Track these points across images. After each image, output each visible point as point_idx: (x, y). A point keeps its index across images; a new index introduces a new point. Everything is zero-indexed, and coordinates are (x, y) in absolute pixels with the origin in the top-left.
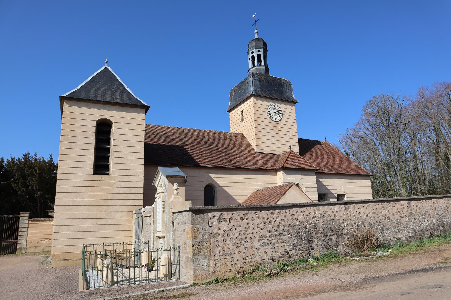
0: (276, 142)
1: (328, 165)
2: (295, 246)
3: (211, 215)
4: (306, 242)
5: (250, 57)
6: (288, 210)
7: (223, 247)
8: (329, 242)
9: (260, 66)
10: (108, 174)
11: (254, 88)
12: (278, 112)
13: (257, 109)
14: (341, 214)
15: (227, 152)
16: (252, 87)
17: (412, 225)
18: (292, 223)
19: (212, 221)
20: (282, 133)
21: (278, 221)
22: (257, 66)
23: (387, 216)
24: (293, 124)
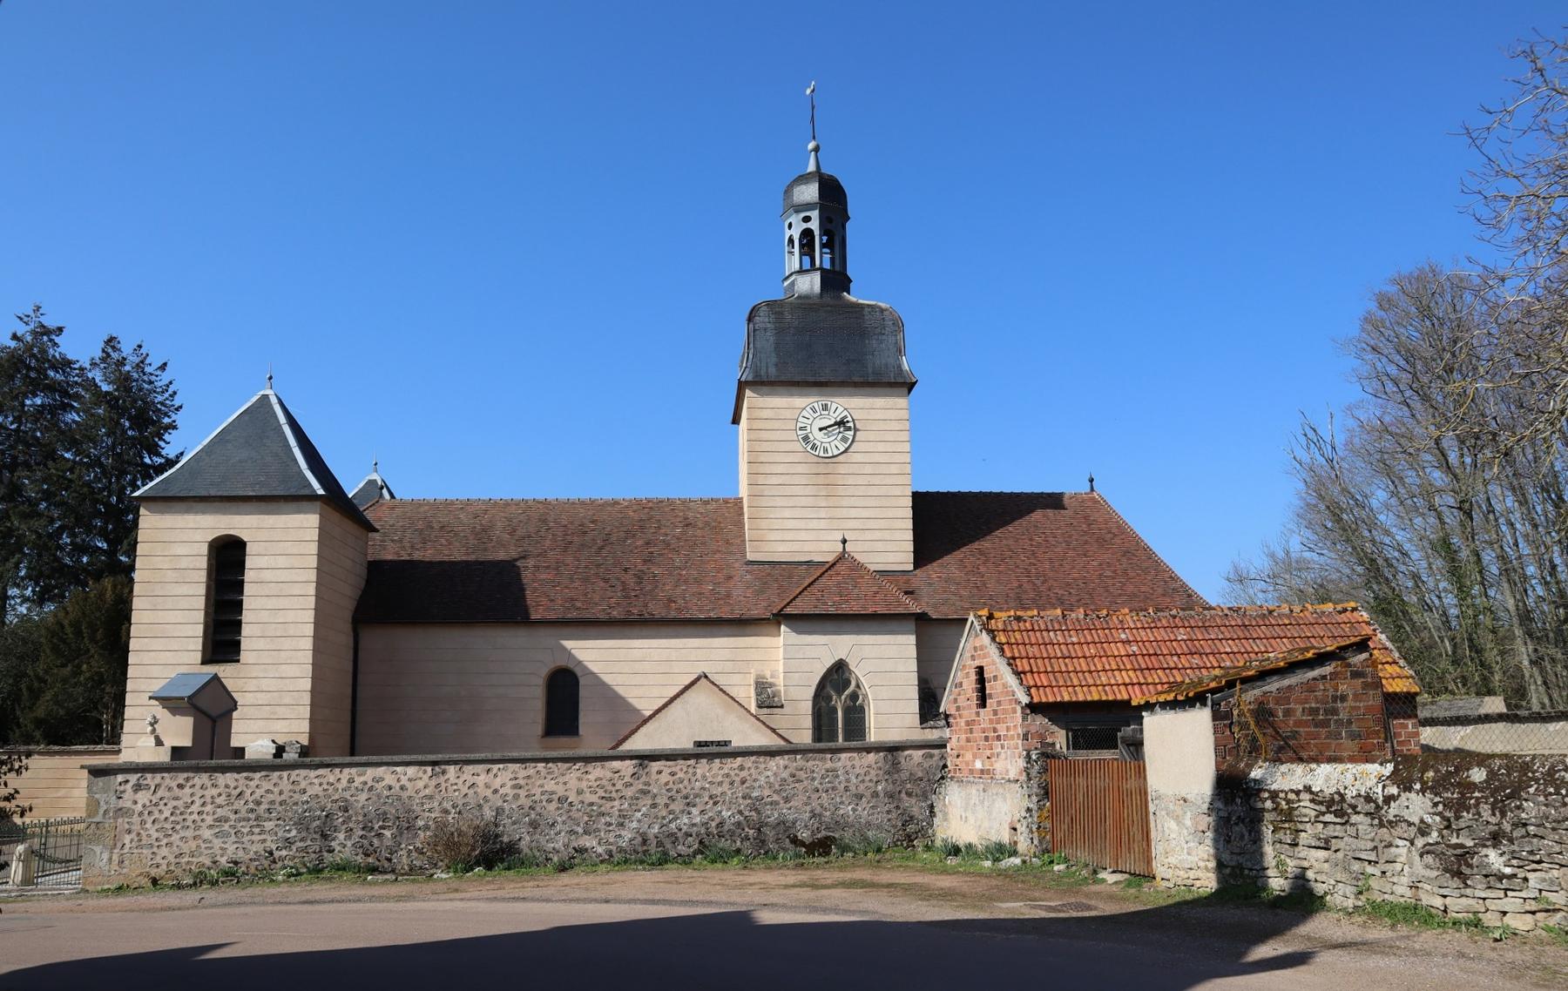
2: (289, 843)
3: (120, 778)
4: (317, 836)
6: (285, 774)
7: (139, 834)
8: (376, 842)
10: (238, 661)
14: (420, 784)
17: (639, 821)
18: (291, 797)
19: (122, 788)
21: (259, 792)
23: (560, 794)
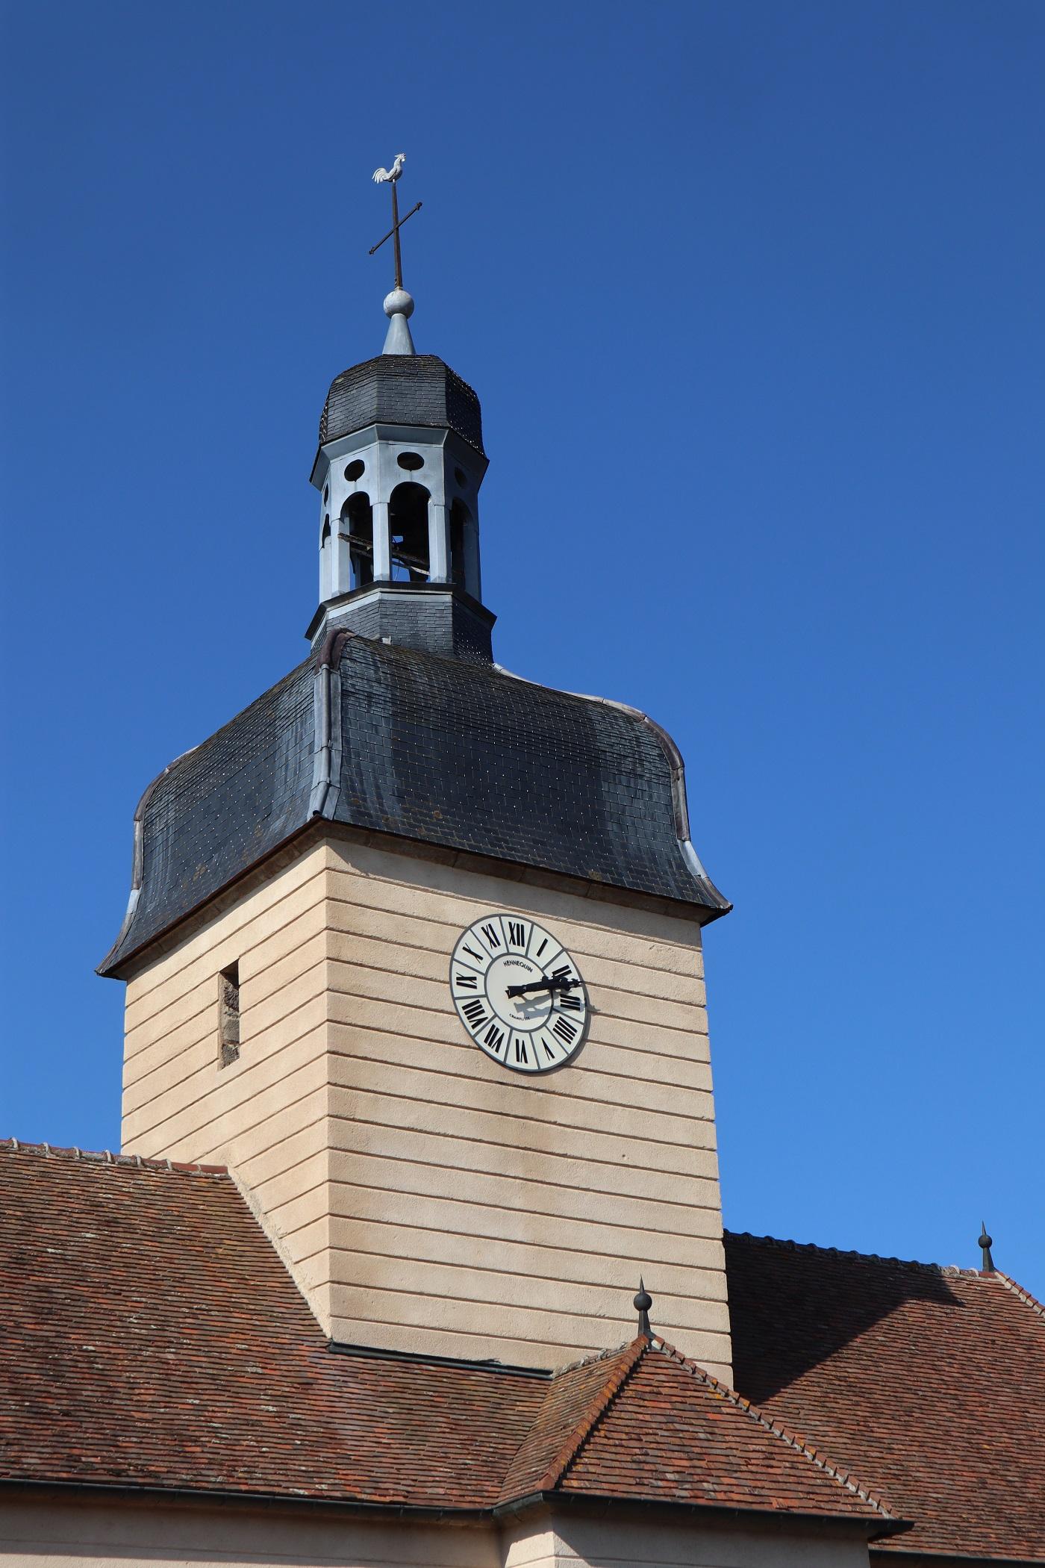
0: (518, 1258)
1: (1001, 1487)
5: (335, 508)
9: (419, 583)
11: (337, 760)
12: (545, 984)
13: (355, 951)
15: (46, 1331)
16: (324, 753)
20: (582, 1174)
22: (391, 584)
24: (685, 1102)
